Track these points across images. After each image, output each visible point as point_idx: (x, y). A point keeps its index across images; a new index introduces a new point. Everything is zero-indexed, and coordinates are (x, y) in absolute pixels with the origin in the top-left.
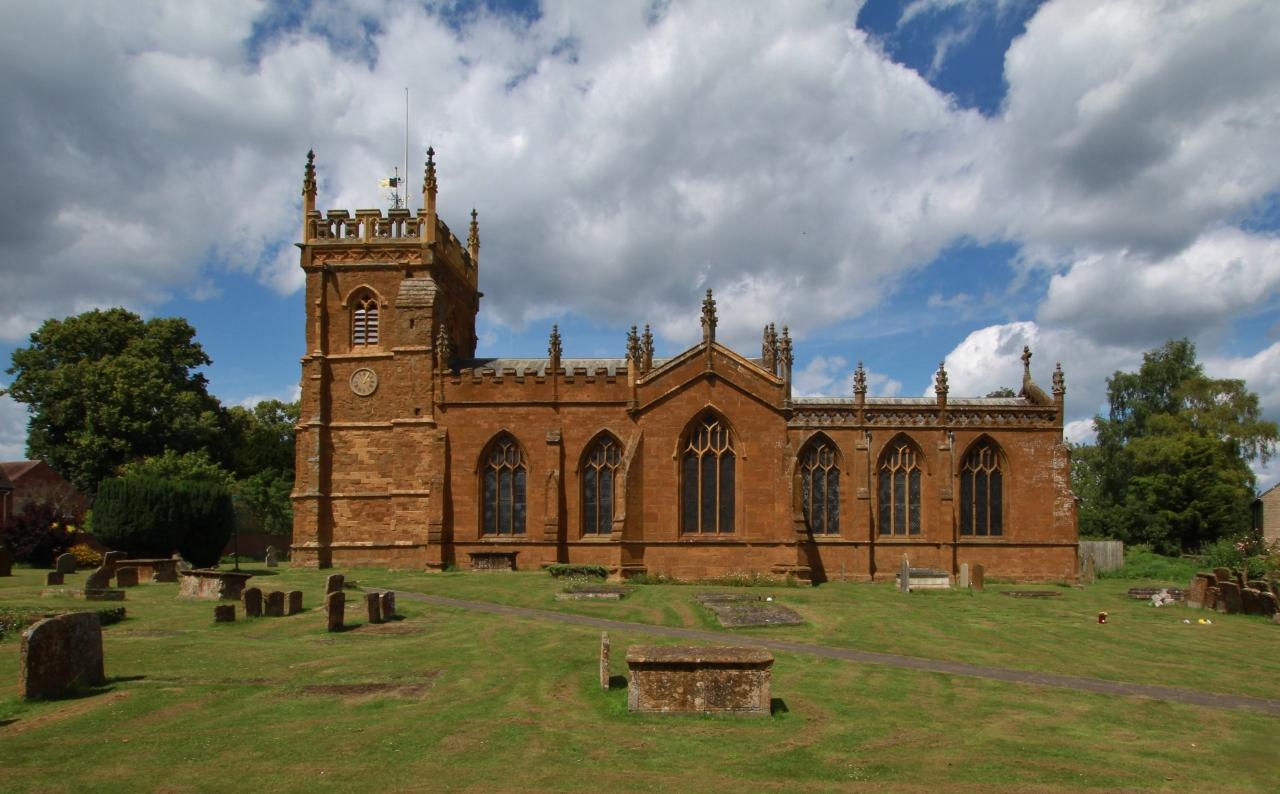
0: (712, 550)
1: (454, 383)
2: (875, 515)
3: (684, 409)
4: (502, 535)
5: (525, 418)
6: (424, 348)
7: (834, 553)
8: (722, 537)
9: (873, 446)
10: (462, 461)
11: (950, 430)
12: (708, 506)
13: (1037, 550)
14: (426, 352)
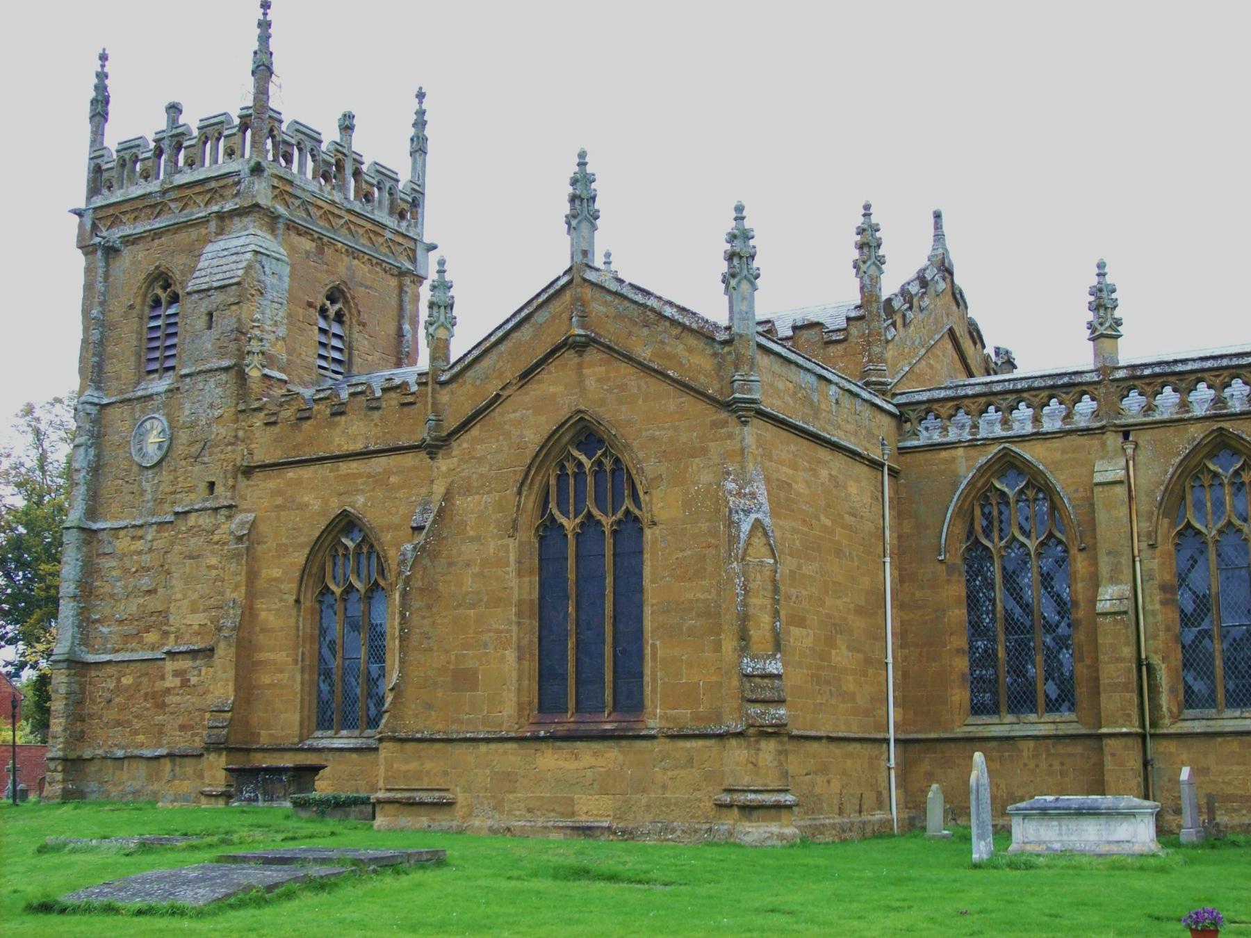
3: (528, 423)
4: (344, 733)
5: (380, 480)
7: (1057, 766)
9: (1153, 468)
10: (276, 579)
14: (227, 369)
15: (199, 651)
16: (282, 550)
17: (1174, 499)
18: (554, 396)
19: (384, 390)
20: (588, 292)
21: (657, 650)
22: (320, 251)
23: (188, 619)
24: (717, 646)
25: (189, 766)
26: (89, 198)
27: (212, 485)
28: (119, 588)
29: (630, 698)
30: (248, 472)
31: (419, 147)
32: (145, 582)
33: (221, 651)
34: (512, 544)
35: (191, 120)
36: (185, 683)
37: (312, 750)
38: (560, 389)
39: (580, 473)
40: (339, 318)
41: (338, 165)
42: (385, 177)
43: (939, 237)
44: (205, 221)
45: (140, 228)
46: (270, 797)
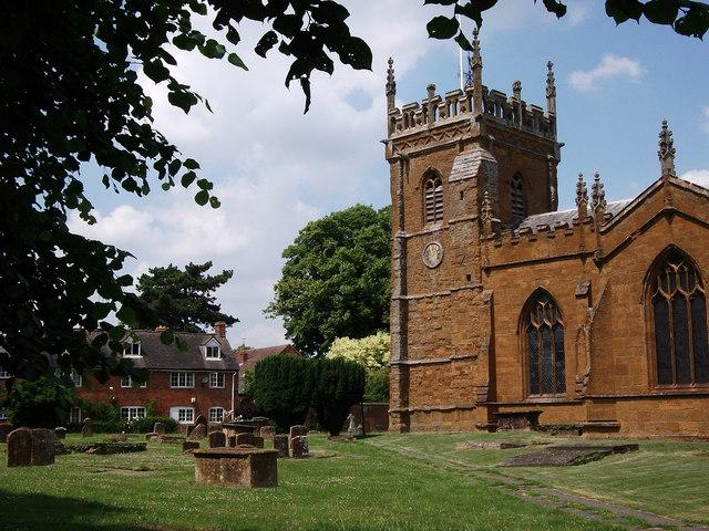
0: (684, 403)
1: (496, 247)
3: (645, 252)
5: (557, 272)
6: (472, 216)
14: (473, 220)
15: (468, 358)
18: (657, 237)
19: (556, 228)
20: (672, 188)
22: (509, 154)
23: (461, 342)
25: (467, 413)
26: (389, 135)
27: (469, 277)
28: (421, 327)
30: (488, 270)
31: (551, 95)
32: (435, 324)
33: (481, 357)
34: (642, 307)
35: (441, 92)
36: (462, 374)
38: (661, 234)
40: (520, 187)
41: (518, 106)
42: (537, 112)
45: (419, 149)
46: (518, 427)
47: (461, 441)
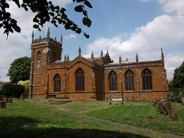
0: (80, 94)
2: (123, 86)
3: (75, 68)
5: (60, 71)
8: (82, 91)
9: (123, 72)
11: (139, 67)
12: (147, 85)
13: (160, 93)
16: (51, 77)
17: (125, 75)
21: (86, 86)
23: (43, 82)
24: (90, 86)
27: (45, 71)
29: (83, 89)
30: (48, 70)
31: (61, 40)
35: (42, 38)
37: (54, 94)
39: (79, 72)
41: (55, 42)
42: (59, 43)
43: (107, 51)
44: (43, 47)
46: (52, 98)
47: (41, 100)
